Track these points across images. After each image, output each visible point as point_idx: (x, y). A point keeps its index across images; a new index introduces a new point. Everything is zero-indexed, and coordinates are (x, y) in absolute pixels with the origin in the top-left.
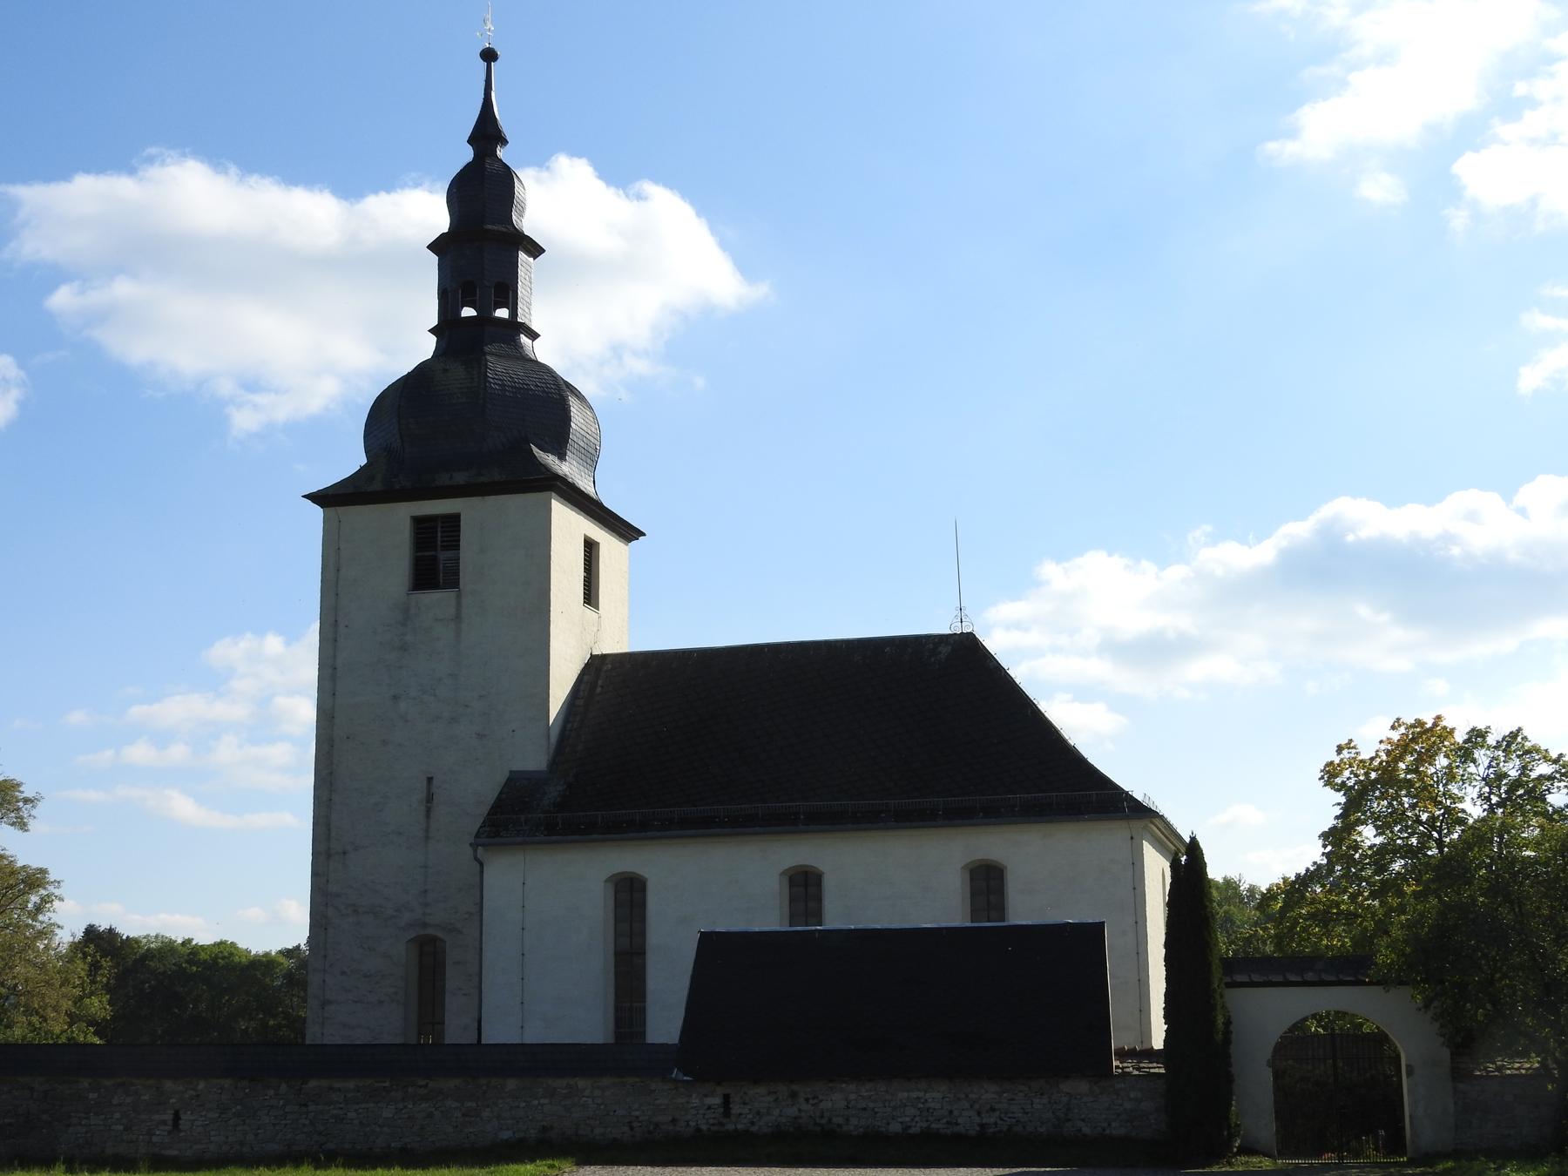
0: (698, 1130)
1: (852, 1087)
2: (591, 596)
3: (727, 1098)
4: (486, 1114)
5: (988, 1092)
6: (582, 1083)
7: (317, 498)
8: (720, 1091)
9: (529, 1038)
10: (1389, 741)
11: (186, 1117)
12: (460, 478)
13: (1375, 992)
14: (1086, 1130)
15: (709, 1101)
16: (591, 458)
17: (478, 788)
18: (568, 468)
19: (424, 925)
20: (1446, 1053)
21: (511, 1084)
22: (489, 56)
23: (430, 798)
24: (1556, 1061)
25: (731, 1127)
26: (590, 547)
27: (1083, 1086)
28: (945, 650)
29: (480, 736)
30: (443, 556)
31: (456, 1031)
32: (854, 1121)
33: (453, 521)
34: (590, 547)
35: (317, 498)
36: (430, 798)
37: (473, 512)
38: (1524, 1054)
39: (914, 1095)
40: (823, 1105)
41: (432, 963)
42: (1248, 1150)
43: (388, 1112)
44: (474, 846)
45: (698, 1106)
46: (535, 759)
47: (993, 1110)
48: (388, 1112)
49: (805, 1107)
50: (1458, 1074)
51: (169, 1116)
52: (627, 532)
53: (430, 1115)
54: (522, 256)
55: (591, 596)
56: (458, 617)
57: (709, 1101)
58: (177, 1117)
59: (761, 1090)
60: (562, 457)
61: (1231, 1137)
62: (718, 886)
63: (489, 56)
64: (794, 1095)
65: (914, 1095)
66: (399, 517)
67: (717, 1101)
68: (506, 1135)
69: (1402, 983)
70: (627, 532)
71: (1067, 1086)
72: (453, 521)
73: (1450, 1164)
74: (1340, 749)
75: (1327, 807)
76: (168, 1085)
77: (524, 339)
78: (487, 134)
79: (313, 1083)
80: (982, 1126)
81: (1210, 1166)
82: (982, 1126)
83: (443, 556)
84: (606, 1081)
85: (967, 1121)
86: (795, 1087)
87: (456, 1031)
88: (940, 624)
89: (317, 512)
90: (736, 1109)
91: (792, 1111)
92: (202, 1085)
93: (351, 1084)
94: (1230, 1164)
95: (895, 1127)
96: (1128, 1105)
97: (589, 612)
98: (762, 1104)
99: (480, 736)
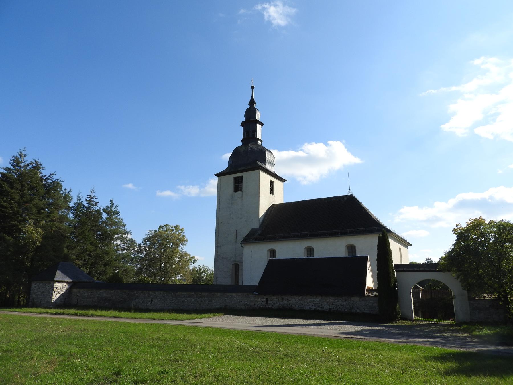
0: (260, 307)
1: (297, 297)
2: (272, 192)
3: (267, 299)
4: (213, 301)
5: (331, 300)
6: (234, 294)
7: (217, 175)
8: (265, 297)
9: (252, 284)
10: (468, 223)
11: (154, 300)
12: (243, 168)
13: (441, 273)
14: (358, 311)
15: (263, 300)
16: (273, 164)
17: (245, 232)
18: (268, 166)
19: (235, 261)
20: (466, 292)
21: (219, 294)
22: (252, 87)
23: (237, 235)
24: (502, 295)
25: (268, 307)
26: (272, 183)
27: (357, 299)
28: (346, 199)
29: (246, 221)
30: (240, 185)
31: (240, 283)
32: (297, 306)
33: (241, 177)
34: (272, 183)
35: (217, 175)
36: (237, 235)
37: (244, 175)
38: (492, 293)
39: (312, 300)
40: (290, 302)
41: (237, 268)
42: (402, 318)
43: (193, 300)
44: (241, 244)
45: (260, 301)
46: (256, 226)
47: (333, 304)
48: (193, 300)
49: (285, 302)
50: (470, 299)
51: (150, 300)
52: (282, 180)
53: (202, 301)
54: (258, 125)
55: (272, 192)
56: (242, 197)
57: (263, 300)
58: (152, 300)
59: (275, 297)
60: (265, 164)
61: (397, 314)
62: (291, 250)
63: (252, 87)
64: (283, 299)
65: (312, 300)
66: (231, 177)
67: (265, 300)
68: (217, 307)
69: (449, 271)
70: (282, 180)
71: (353, 299)
72: (241, 177)
73: (466, 326)
74: (457, 225)
75: (454, 238)
76: (151, 292)
77: (258, 141)
78: (252, 102)
79: (178, 293)
80: (330, 309)
81: (389, 323)
82: (330, 309)
83: (240, 185)
84: (239, 294)
85: (326, 307)
86: (283, 297)
87: (240, 283)
88: (344, 193)
89: (216, 178)
90: (269, 302)
91: (282, 303)
92: (157, 293)
93: (186, 294)
94: (396, 323)
95: (308, 308)
96: (370, 304)
97: (271, 195)
98: (275, 301)
99: (246, 221)
